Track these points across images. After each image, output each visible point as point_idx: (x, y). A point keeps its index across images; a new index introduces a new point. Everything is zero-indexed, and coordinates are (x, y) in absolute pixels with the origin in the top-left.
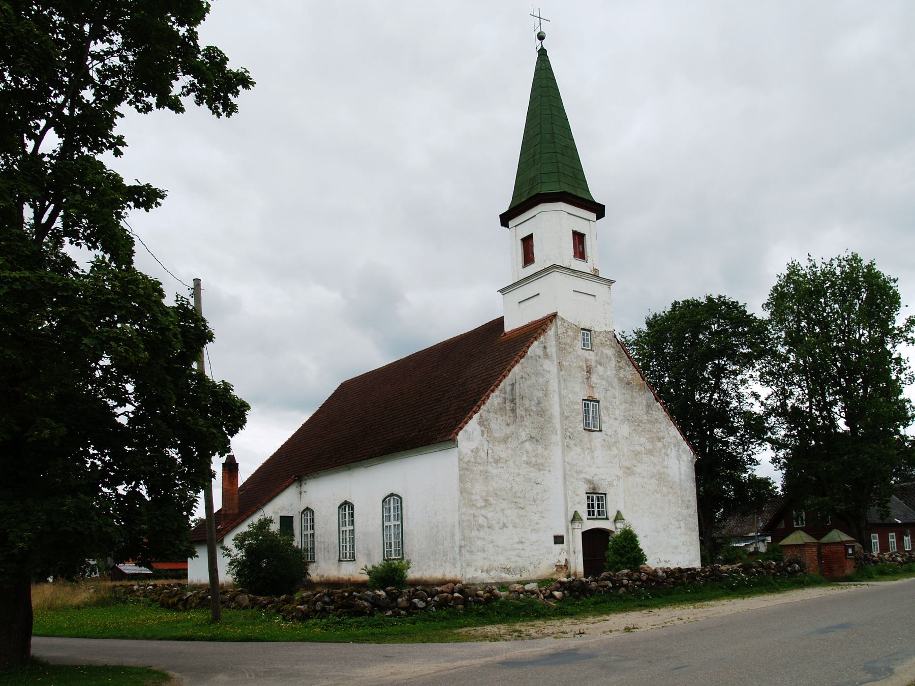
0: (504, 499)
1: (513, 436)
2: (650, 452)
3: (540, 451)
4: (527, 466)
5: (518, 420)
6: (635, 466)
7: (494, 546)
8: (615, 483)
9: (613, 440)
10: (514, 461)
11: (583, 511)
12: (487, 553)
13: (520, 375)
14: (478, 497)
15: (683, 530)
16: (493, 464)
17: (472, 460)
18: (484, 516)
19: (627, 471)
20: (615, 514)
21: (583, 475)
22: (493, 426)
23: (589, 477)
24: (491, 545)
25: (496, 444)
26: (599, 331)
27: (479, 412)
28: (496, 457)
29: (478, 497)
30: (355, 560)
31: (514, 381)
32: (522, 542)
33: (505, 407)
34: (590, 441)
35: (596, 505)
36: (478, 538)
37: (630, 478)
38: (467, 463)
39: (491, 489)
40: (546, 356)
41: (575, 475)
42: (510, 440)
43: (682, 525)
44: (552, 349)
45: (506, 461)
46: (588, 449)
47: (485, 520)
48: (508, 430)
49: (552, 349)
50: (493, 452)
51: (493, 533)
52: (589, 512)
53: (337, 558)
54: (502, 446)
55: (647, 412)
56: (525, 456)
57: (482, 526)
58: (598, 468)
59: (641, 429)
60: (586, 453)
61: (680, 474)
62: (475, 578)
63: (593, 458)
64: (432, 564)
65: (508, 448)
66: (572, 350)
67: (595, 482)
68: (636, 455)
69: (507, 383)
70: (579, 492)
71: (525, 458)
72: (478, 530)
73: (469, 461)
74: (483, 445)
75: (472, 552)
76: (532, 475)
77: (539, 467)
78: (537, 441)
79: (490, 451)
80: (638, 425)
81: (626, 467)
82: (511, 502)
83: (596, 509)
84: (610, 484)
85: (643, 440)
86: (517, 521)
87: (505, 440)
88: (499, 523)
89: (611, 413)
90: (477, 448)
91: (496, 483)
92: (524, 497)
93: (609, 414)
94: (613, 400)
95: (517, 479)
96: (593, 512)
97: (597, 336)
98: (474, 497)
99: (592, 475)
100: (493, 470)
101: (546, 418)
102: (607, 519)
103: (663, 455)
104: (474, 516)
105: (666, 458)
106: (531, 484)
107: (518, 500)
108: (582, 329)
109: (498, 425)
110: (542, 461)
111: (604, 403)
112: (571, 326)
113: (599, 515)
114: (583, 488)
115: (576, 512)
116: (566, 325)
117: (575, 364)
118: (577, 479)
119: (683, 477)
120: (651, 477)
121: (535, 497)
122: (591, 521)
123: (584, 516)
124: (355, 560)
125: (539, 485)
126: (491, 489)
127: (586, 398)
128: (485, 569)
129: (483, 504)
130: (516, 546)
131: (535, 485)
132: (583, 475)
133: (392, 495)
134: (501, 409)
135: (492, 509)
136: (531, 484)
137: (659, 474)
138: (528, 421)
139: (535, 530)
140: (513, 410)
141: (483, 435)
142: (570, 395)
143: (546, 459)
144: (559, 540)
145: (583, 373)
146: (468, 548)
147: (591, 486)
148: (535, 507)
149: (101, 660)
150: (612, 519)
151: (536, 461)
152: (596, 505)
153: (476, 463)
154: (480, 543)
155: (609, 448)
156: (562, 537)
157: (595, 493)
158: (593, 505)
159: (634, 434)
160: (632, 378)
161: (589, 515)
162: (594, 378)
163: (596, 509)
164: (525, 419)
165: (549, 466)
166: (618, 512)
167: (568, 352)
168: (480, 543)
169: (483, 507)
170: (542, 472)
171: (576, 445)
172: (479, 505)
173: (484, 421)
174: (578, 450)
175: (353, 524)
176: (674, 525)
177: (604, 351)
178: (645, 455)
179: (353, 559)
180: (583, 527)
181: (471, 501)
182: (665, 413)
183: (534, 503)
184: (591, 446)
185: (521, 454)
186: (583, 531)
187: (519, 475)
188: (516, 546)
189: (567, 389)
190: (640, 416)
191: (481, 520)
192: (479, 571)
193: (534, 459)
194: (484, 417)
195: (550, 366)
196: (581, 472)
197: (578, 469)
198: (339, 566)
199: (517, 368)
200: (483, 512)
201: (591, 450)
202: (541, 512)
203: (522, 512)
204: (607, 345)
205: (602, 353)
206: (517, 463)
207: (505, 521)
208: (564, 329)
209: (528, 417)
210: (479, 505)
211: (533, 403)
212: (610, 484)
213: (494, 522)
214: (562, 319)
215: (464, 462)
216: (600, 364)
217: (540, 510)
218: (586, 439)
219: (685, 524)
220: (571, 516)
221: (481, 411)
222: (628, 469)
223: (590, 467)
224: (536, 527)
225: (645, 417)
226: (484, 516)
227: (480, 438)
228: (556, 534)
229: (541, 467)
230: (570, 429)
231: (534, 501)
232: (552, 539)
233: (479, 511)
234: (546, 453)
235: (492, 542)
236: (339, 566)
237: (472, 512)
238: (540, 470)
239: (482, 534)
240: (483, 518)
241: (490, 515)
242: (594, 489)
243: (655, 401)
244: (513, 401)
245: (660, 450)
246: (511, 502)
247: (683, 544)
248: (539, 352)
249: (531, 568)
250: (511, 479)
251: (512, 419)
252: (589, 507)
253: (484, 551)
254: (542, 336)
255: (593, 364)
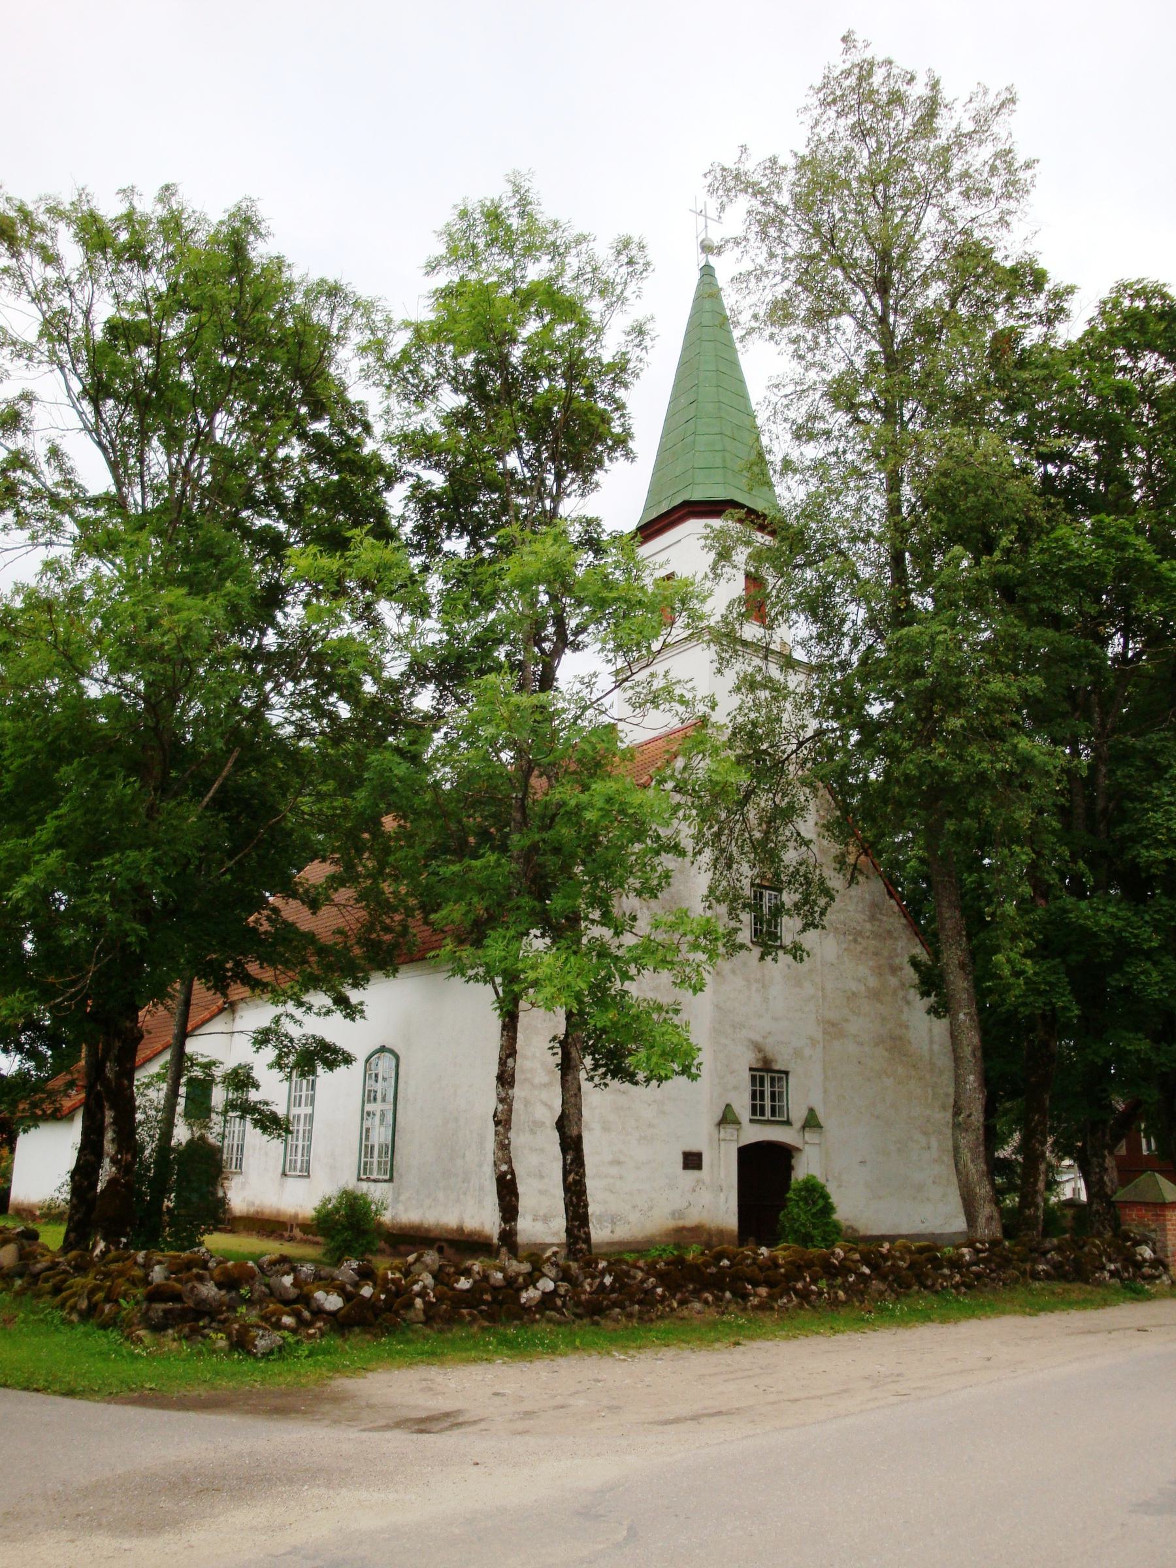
11: (742, 1106)
20: (804, 1113)
23: (757, 1038)
30: (308, 1176)
35: (767, 1095)
46: (757, 981)
52: (754, 1107)
53: (280, 1170)
55: (872, 918)
59: (859, 948)
61: (931, 1042)
63: (766, 1000)
64: (441, 1195)
67: (768, 1048)
72: (532, 1132)
81: (829, 1022)
83: (768, 1103)
84: (798, 1053)
96: (762, 1107)
102: (788, 1123)
105: (906, 1009)
113: (773, 1114)
114: (746, 1060)
115: (728, 1106)
119: (936, 1047)
120: (877, 1045)
122: (757, 1127)
123: (744, 1113)
124: (308, 1176)
133: (383, 1049)
144: (692, 1161)
147: (760, 1056)
150: (798, 1122)
152: (767, 1095)
158: (762, 1093)
161: (754, 1112)
163: (768, 1103)
166: (811, 1111)
171: (733, 972)
172: (537, 1081)
175: (312, 1103)
179: (306, 1173)
182: (904, 921)
186: (741, 1144)
198: (282, 1185)
210: (537, 1081)
220: (718, 1115)
222: (833, 1025)
225: (868, 926)
226: (546, 1105)
228: (688, 1149)
232: (680, 1160)
236: (282, 1185)
249: (634, 1217)
252: (754, 1097)
253: (542, 1177)
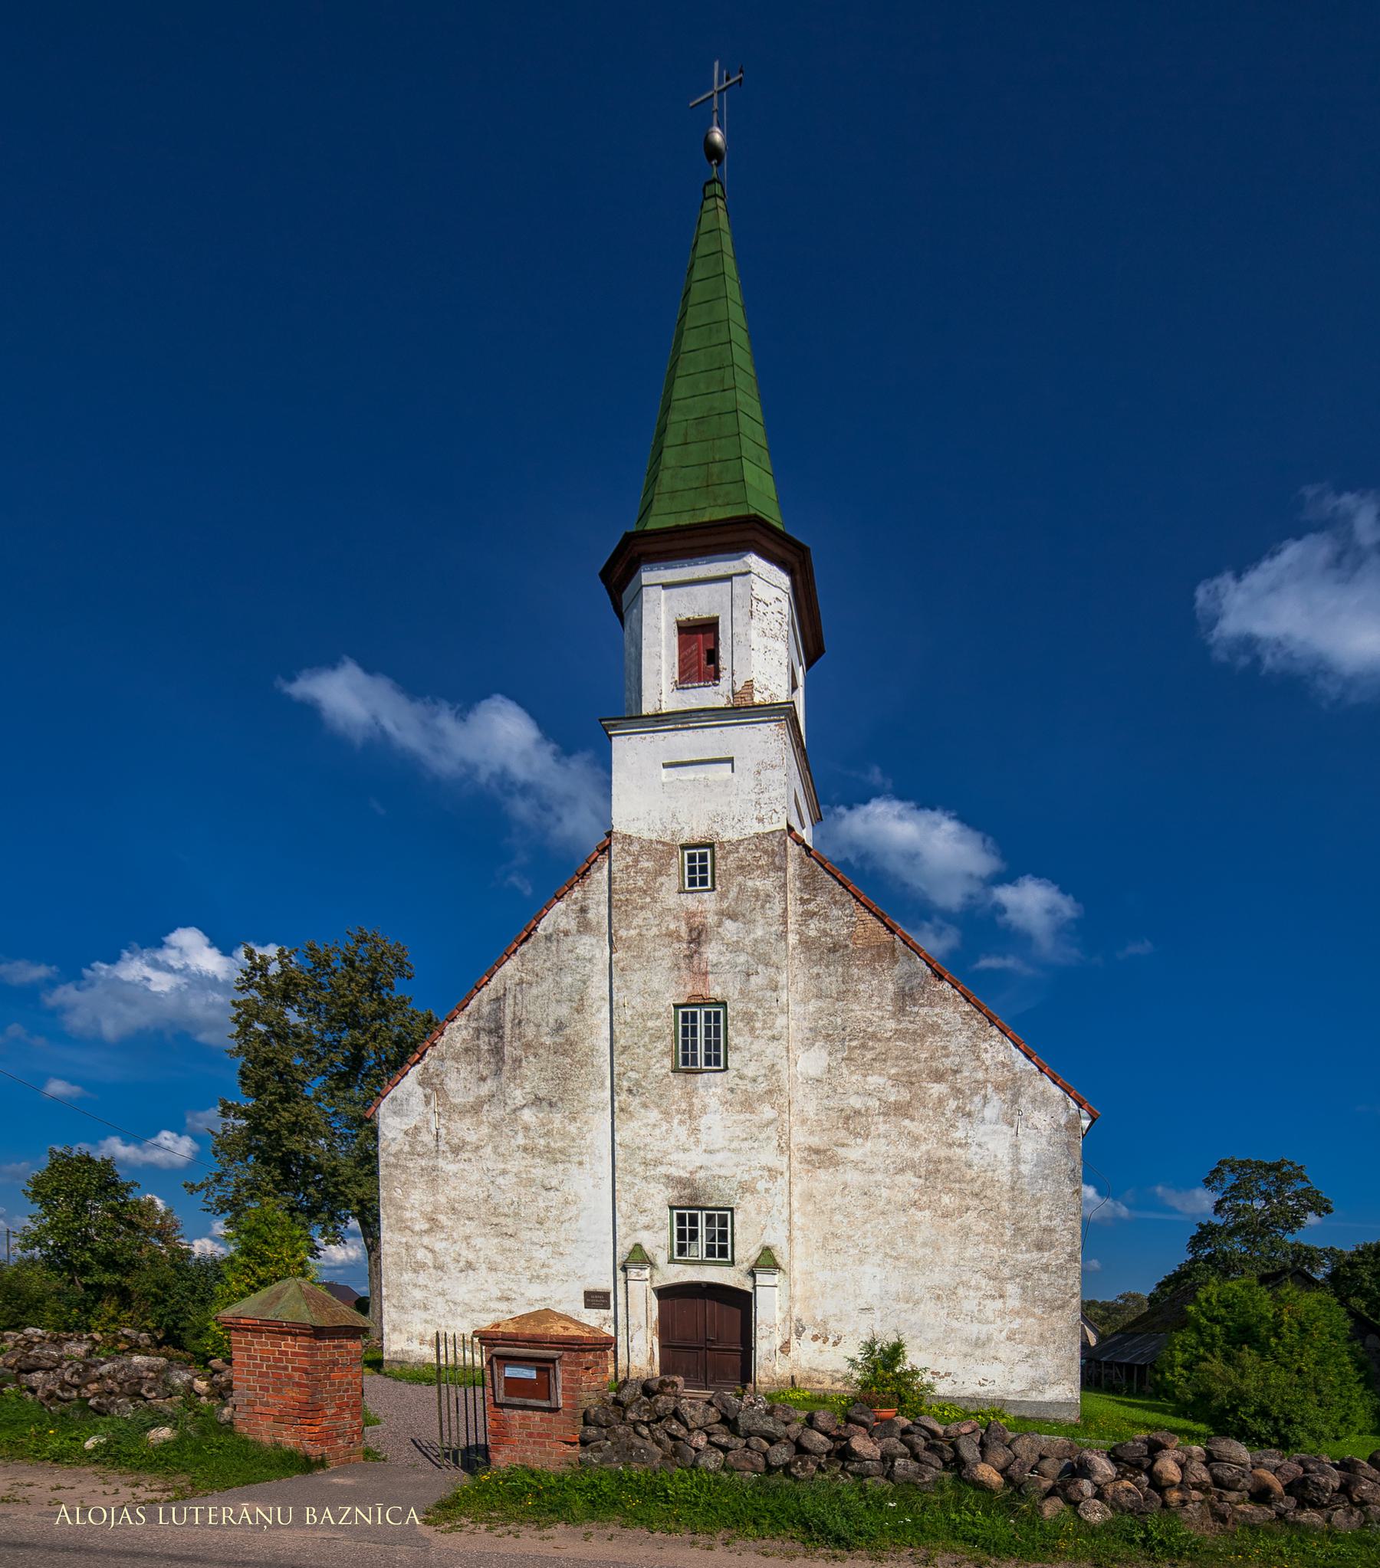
0: (470, 1219)
1: (495, 1100)
2: (901, 1110)
3: (557, 1124)
4: (525, 1155)
5: (506, 1068)
6: (843, 1145)
7: (447, 1301)
8: (761, 1186)
9: (763, 1087)
10: (496, 1148)
11: (658, 1241)
12: (431, 1312)
13: (517, 978)
14: (416, 1214)
15: (1014, 1303)
16: (448, 1155)
17: (407, 1148)
18: (426, 1248)
19: (814, 1157)
21: (662, 1170)
22: (452, 1084)
24: (440, 1299)
25: (456, 1116)
26: (736, 837)
27: (423, 1063)
28: (456, 1141)
29: (416, 1214)
31: (502, 992)
32: (508, 1299)
33: (478, 1046)
34: (690, 1095)
36: (415, 1285)
37: (821, 1174)
38: (395, 1155)
39: (443, 1200)
40: (585, 927)
41: (640, 1169)
42: (486, 1107)
43: (1011, 1289)
44: (598, 912)
45: (478, 1148)
47: (430, 1255)
48: (485, 1089)
49: (598, 912)
50: (448, 1134)
51: (445, 1278)
54: (468, 1121)
56: (520, 1135)
57: (421, 1266)
58: (710, 1152)
59: (869, 1055)
60: (676, 1121)
61: (1017, 1161)
62: (407, 1352)
65: (482, 1122)
66: (648, 900)
67: (699, 1183)
68: (848, 1118)
69: (485, 998)
70: (648, 1205)
71: (521, 1140)
72: (415, 1271)
73: (401, 1151)
74: (428, 1122)
75: (403, 1308)
76: (538, 1173)
77: (553, 1156)
78: (551, 1105)
79: (443, 1131)
80: (863, 1046)
82: (485, 1224)
85: (874, 1080)
86: (499, 1259)
87: (476, 1108)
88: (459, 1262)
89: (758, 1025)
90: (416, 1128)
91: (455, 1188)
92: (517, 1214)
93: (752, 1029)
94: (769, 993)
95: (500, 1180)
97: (729, 852)
98: (408, 1215)
99: (690, 1169)
100: (448, 1166)
101: (578, 1056)
103: (948, 1115)
104: (408, 1247)
106: (533, 1190)
107: (502, 1220)
108: (684, 847)
109: (460, 1083)
110: (559, 1144)
111: (740, 1006)
112: (647, 848)
116: (635, 848)
117: (655, 931)
118: (645, 1178)
121: (542, 1215)
123: (661, 1258)
125: (552, 1193)
126: (443, 1200)
127: (683, 1000)
128: (428, 1338)
129: (426, 1226)
130: (494, 1305)
131: (544, 1193)
132: (662, 1170)
134: (467, 1050)
135: (443, 1236)
136: (533, 1190)
137: (929, 1160)
138: (530, 1068)
139: (538, 1277)
140: (497, 1051)
141: (427, 1103)
142: (637, 1001)
143: (574, 1140)
145: (676, 945)
146: (394, 1301)
148: (541, 1233)
149: (515, 1354)
151: (548, 1146)
153: (413, 1154)
154: (418, 1294)
155: (748, 1105)
156: (606, 1295)
157: (702, 1209)
159: (845, 1071)
160: (850, 936)
162: (711, 952)
164: (524, 1064)
165: (581, 1154)
167: (635, 908)
168: (418, 1294)
169: (425, 1232)
170: (561, 1167)
171: (645, 1106)
172: (417, 1228)
173: (431, 1078)
174: (654, 1115)
176: (978, 1288)
177: (750, 883)
178: (881, 1118)
180: (657, 1277)
181: (403, 1221)
183: (538, 1226)
184: (691, 1105)
185: (510, 1133)
187: (504, 1172)
188: (494, 1305)
189: (628, 988)
190: (871, 1022)
191: (421, 1255)
192: (416, 1342)
193: (542, 1142)
194: (431, 1070)
195: (593, 948)
196: (657, 1163)
197: (649, 1156)
199: (510, 967)
200: (426, 1240)
201: (690, 1114)
202: (556, 1244)
203: (508, 1243)
204: (759, 867)
205: (742, 889)
206: (501, 1150)
207: (471, 1257)
208: (629, 859)
209: (531, 1058)
210: (417, 1228)
211: (545, 1029)
212: (746, 1188)
213: (448, 1259)
214: (625, 837)
215: (389, 1154)
216: (733, 917)
217: (553, 1240)
218: (677, 1093)
219: (1024, 1288)
221: (427, 1059)
222: (817, 1152)
223: (685, 1150)
224: (543, 1272)
225: (891, 1025)
226: (426, 1248)
227: (421, 1108)
229: (558, 1156)
230: (631, 1074)
231: (541, 1224)
233: (417, 1238)
234: (572, 1129)
235: (443, 1294)
237: (404, 1240)
238: (556, 1163)
239: (422, 1279)
240: (423, 1250)
241: (439, 1246)
242: (694, 1197)
243: (933, 980)
244: (496, 1031)
245: (941, 1100)
246: (485, 1224)
247: (1009, 1338)
248: (569, 923)
250: (487, 1181)
251: (492, 1067)
253: (426, 1308)
254: (576, 889)
255: (712, 920)
